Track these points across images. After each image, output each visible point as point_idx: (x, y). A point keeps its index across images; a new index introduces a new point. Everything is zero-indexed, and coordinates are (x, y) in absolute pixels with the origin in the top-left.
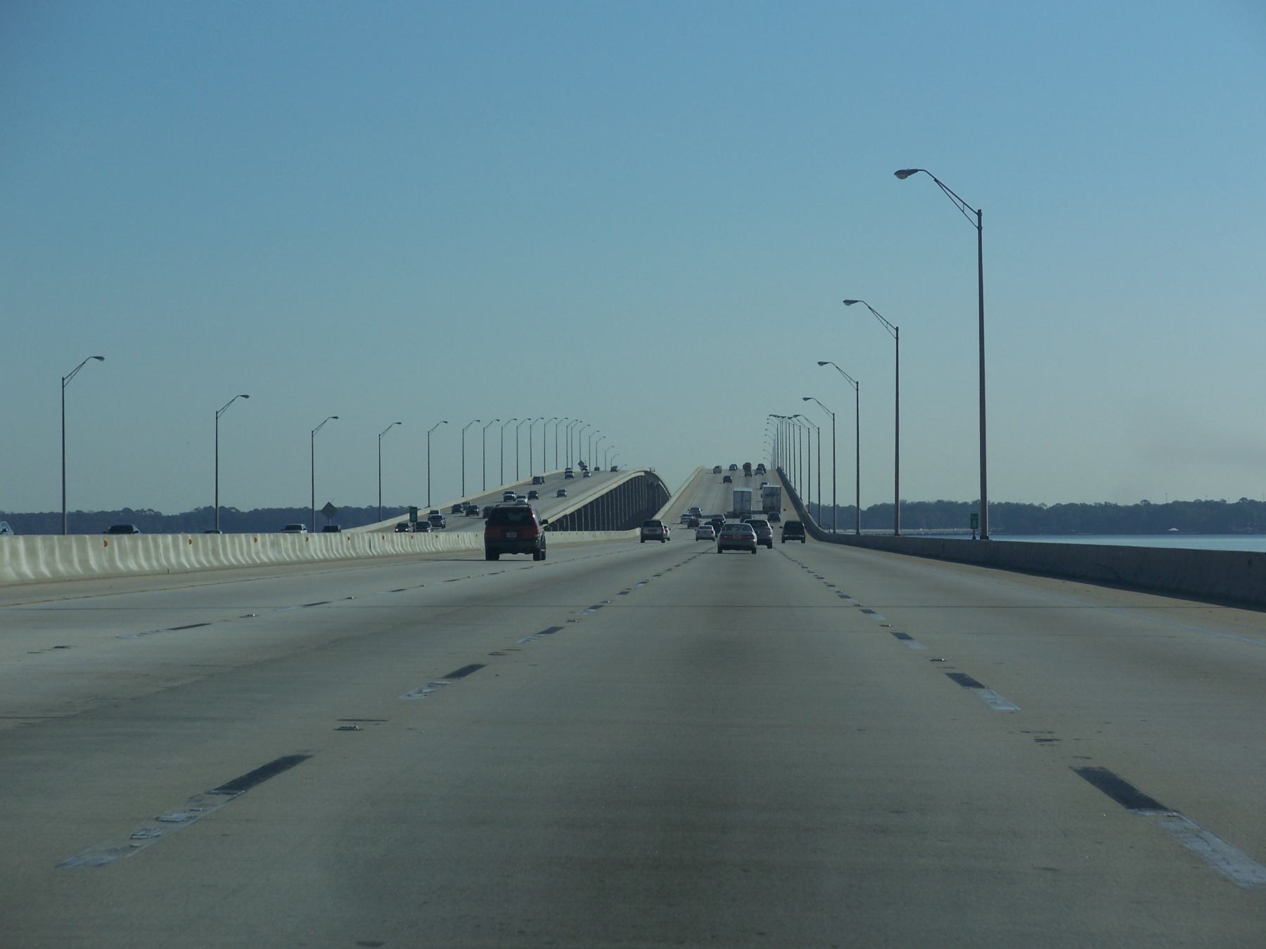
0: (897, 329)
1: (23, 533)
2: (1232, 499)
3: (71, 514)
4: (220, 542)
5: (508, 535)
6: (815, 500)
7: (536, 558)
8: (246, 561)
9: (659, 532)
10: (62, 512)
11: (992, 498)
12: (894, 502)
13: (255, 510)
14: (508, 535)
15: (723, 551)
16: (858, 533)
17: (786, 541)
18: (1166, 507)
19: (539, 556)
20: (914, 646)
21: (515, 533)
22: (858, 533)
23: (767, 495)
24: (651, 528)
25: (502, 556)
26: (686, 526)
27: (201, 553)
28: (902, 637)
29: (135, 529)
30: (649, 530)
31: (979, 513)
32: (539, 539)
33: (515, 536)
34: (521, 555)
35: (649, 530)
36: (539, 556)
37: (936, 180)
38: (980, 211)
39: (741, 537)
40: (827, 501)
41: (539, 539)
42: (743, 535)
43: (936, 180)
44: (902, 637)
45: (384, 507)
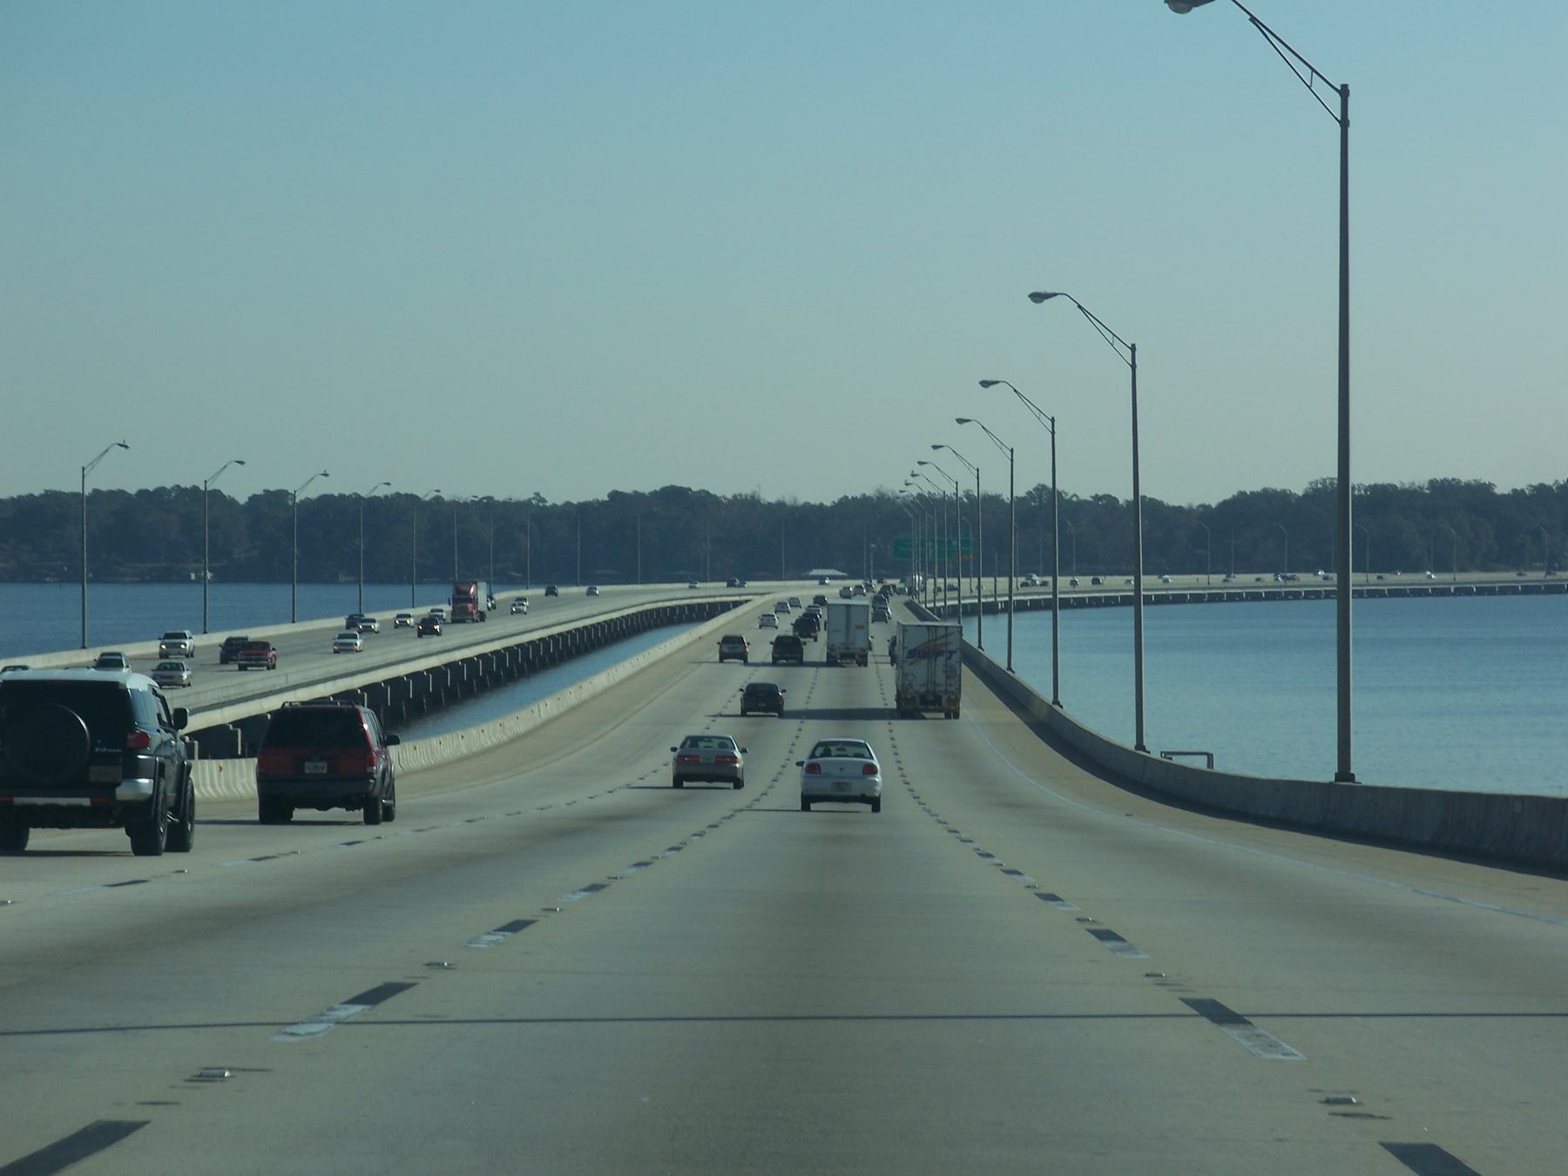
0: (1133, 348)
4: (199, 766)
5: (309, 768)
7: (371, 819)
8: (208, 793)
9: (739, 650)
10: (1333, 472)
11: (1361, 477)
14: (309, 768)
15: (685, 784)
17: (813, 806)
19: (377, 810)
21: (325, 764)
23: (915, 654)
24: (731, 646)
27: (237, 770)
29: (231, 726)
30: (729, 648)
32: (378, 776)
33: (325, 771)
34: (336, 813)
35: (729, 648)
36: (377, 810)
38: (1133, 345)
39: (714, 761)
41: (378, 776)
42: (717, 757)
45: (1155, 507)
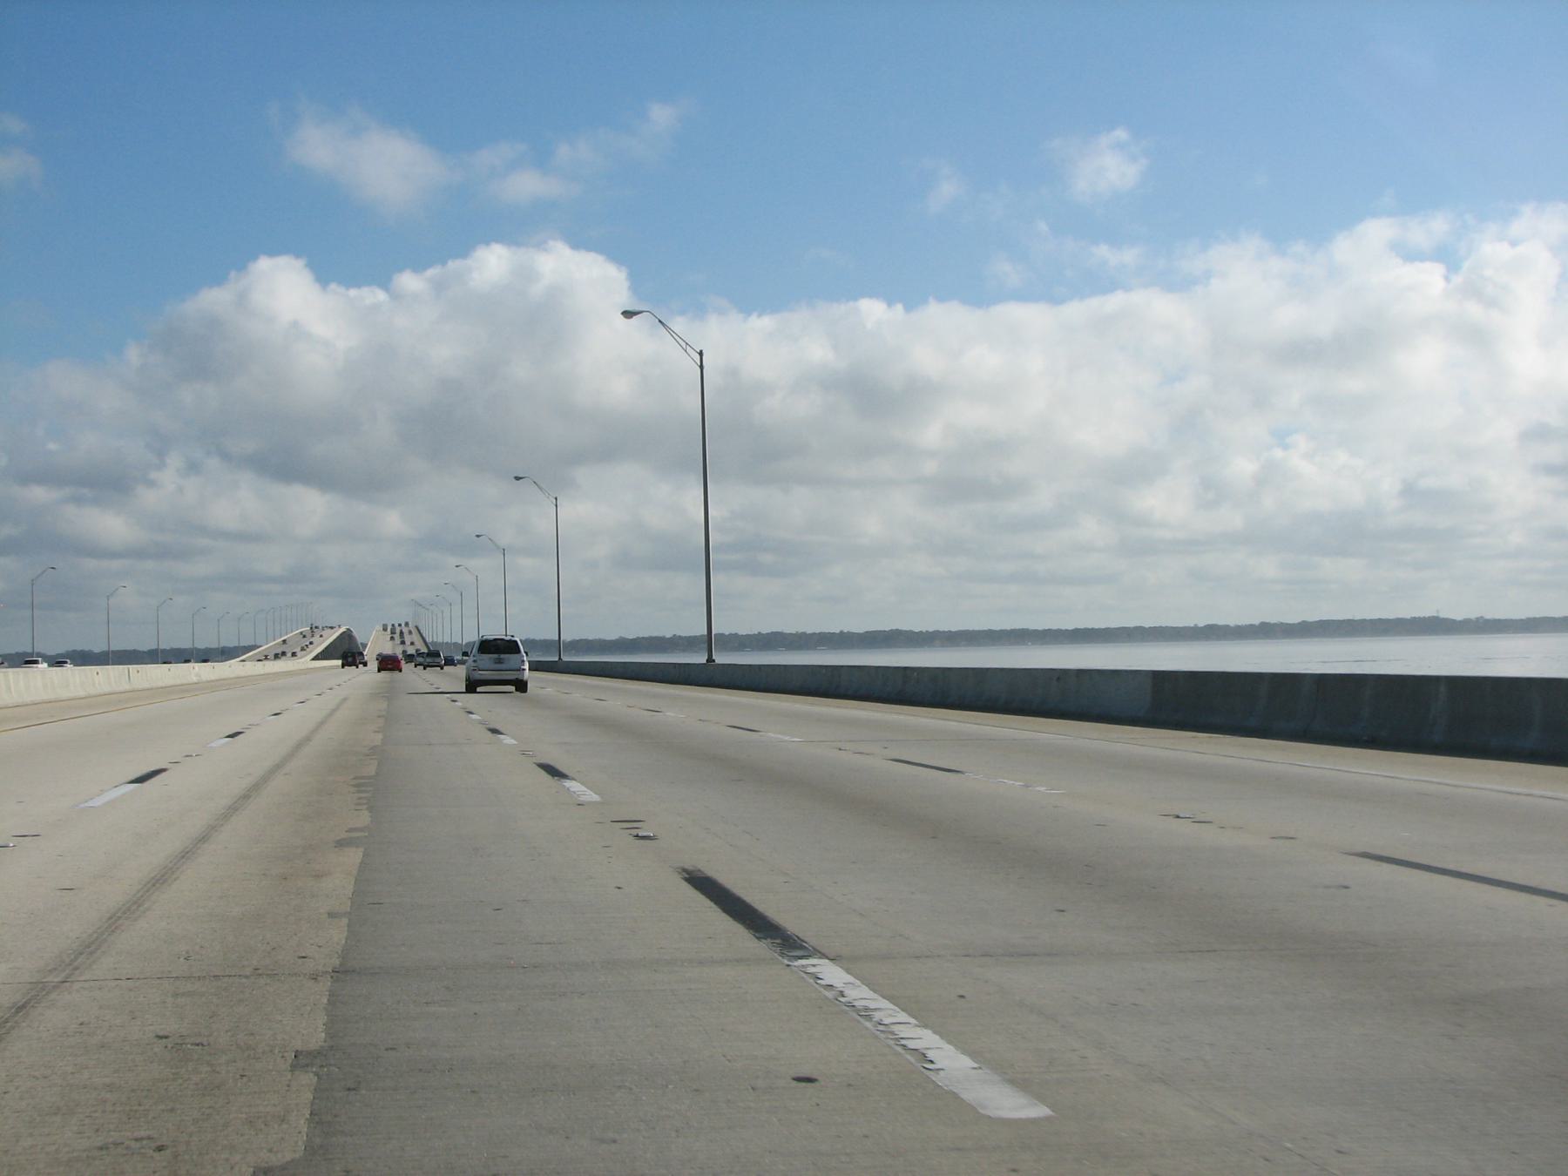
1: (522, 680)
2: (668, 635)
3: (112, 651)
6: (435, 640)
10: (557, 638)
11: (36, 650)
12: (706, 633)
13: (841, 632)
16: (710, 660)
18: (955, 632)
20: (508, 740)
22: (710, 660)
25: (478, 689)
26: (339, 662)
28: (495, 731)
31: (558, 645)
37: (660, 321)
40: (440, 640)
43: (660, 321)
44: (495, 731)
